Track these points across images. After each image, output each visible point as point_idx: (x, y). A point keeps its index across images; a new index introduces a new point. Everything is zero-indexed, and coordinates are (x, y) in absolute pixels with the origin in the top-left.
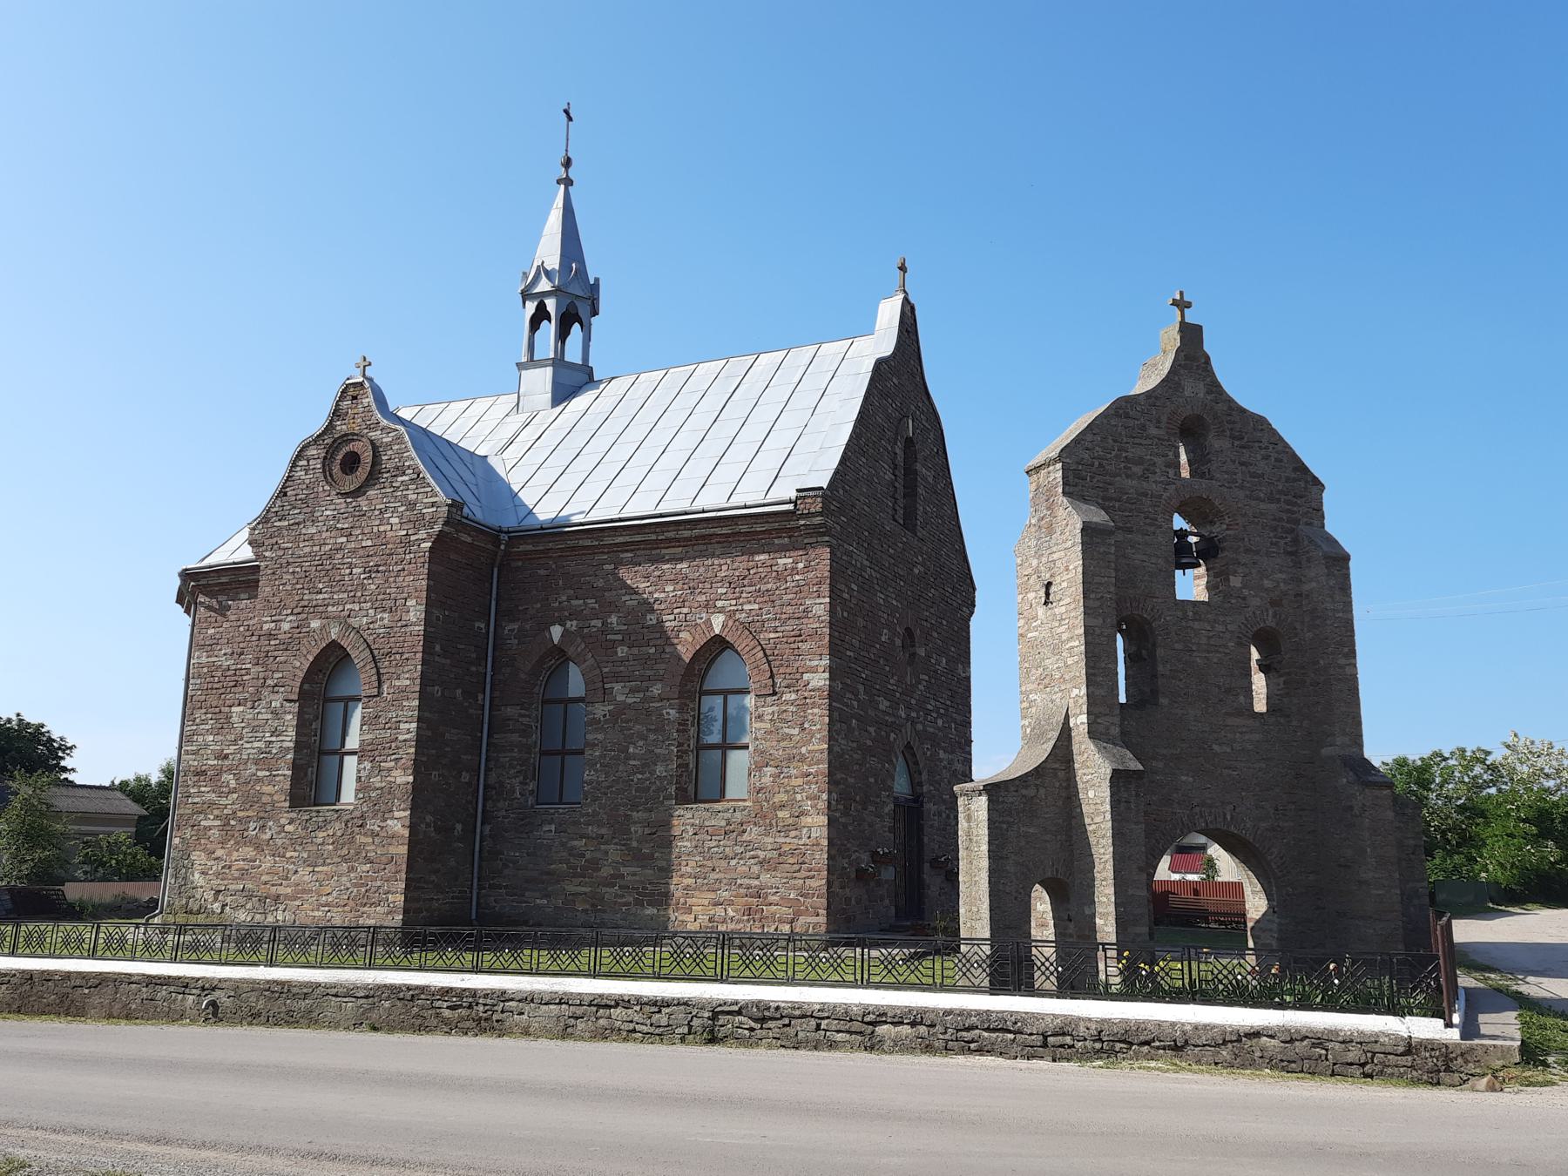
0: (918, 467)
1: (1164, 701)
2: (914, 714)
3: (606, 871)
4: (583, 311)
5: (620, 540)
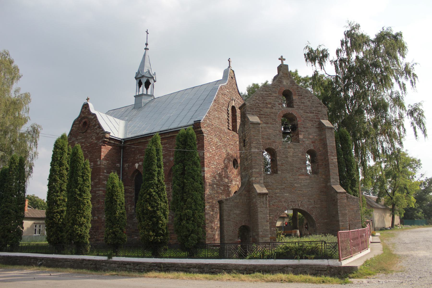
1: (279, 172)
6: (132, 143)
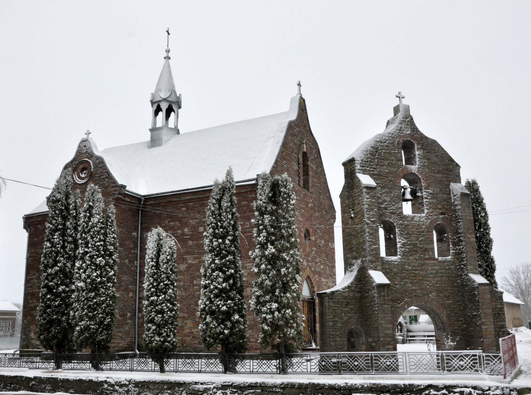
0: (309, 163)
2: (310, 264)
3: (187, 331)
4: (174, 107)
5: (188, 198)
6: (157, 202)
